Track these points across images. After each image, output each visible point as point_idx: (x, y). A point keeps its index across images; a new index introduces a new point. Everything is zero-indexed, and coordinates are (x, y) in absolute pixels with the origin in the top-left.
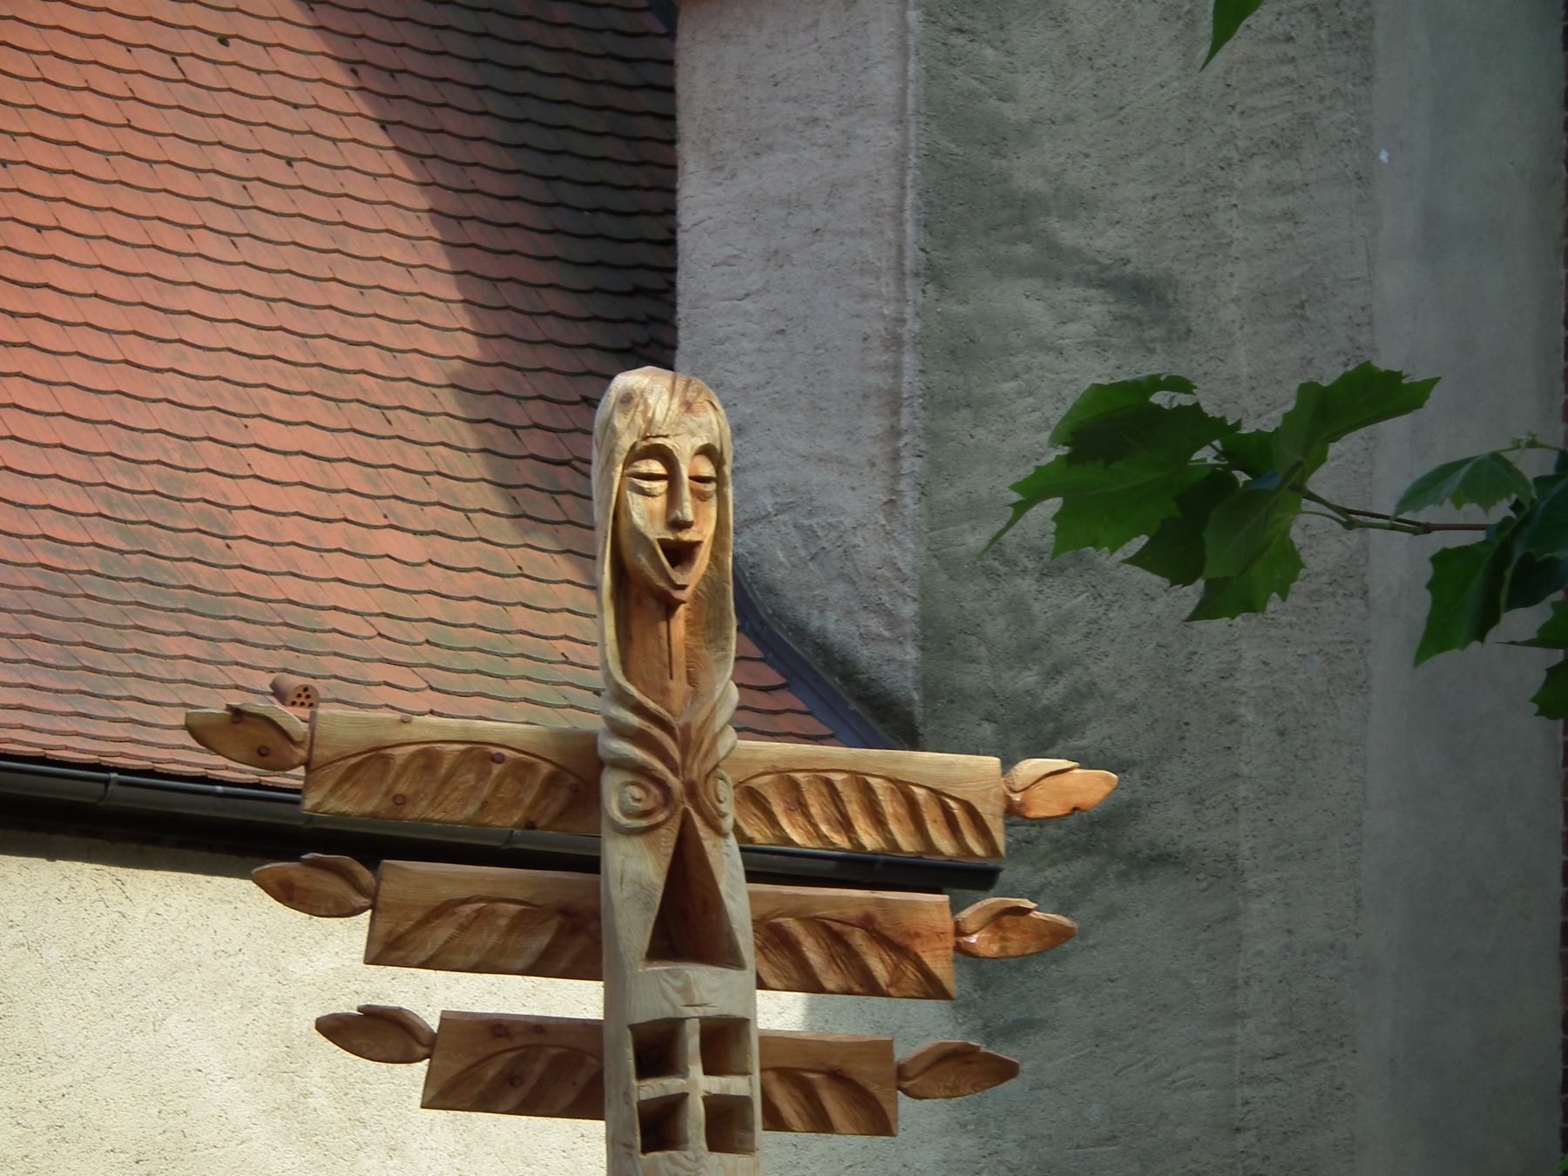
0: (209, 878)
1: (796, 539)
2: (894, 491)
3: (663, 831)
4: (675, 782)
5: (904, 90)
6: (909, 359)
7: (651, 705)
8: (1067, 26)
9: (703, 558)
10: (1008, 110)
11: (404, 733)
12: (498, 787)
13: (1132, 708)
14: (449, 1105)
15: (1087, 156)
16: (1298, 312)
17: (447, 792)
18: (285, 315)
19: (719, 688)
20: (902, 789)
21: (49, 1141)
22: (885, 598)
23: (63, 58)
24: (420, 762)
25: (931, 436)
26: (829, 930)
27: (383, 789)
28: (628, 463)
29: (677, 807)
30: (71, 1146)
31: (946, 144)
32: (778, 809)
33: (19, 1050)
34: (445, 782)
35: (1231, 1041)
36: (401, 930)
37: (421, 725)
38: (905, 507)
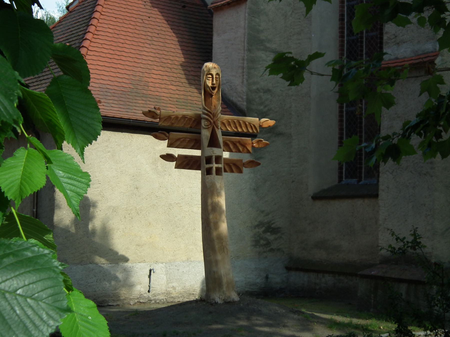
3: (210, 128)
4: (212, 121)
6: (245, 62)
7: (209, 110)
20: (245, 123)
28: (206, 76)
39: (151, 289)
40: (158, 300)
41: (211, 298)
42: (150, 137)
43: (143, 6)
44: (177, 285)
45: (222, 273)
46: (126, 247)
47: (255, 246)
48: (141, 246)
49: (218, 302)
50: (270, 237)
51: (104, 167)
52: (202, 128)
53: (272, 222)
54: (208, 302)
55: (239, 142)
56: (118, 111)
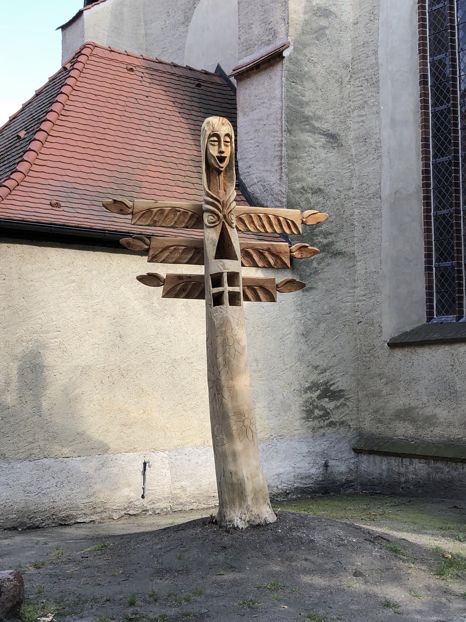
0: (131, 255)
1: (261, 187)
2: (281, 176)
3: (218, 227)
4: (221, 215)
5: (282, 94)
6: (284, 149)
7: (215, 196)
8: (315, 83)
9: (227, 161)
10: (304, 98)
11: (155, 205)
12: (179, 218)
13: (332, 222)
14: (169, 296)
15: (320, 109)
16: (365, 141)
17: (167, 219)
18: (156, 146)
19: (231, 192)
20: (277, 217)
21: (93, 315)
22: (280, 198)
23: (113, 98)
24: (160, 212)
25: (289, 164)
26: (259, 252)
27: (151, 219)
28: (209, 138)
29: (221, 221)
30: (98, 316)
31: (290, 104)
32: (247, 222)
33: (86, 294)
34: (166, 217)
35: (354, 292)
36: (156, 253)
37: (160, 203)
38: (283, 179)
39: (146, 493)
40: (158, 509)
41: (227, 518)
42: (139, 259)
43: (139, 83)
44: (188, 484)
45: (245, 474)
46: (105, 429)
47: (306, 419)
48: (128, 426)
49: (238, 527)
50: (330, 405)
51: (66, 305)
52: (205, 227)
53: (331, 383)
54: (220, 527)
55: (269, 250)
56: (88, 218)
